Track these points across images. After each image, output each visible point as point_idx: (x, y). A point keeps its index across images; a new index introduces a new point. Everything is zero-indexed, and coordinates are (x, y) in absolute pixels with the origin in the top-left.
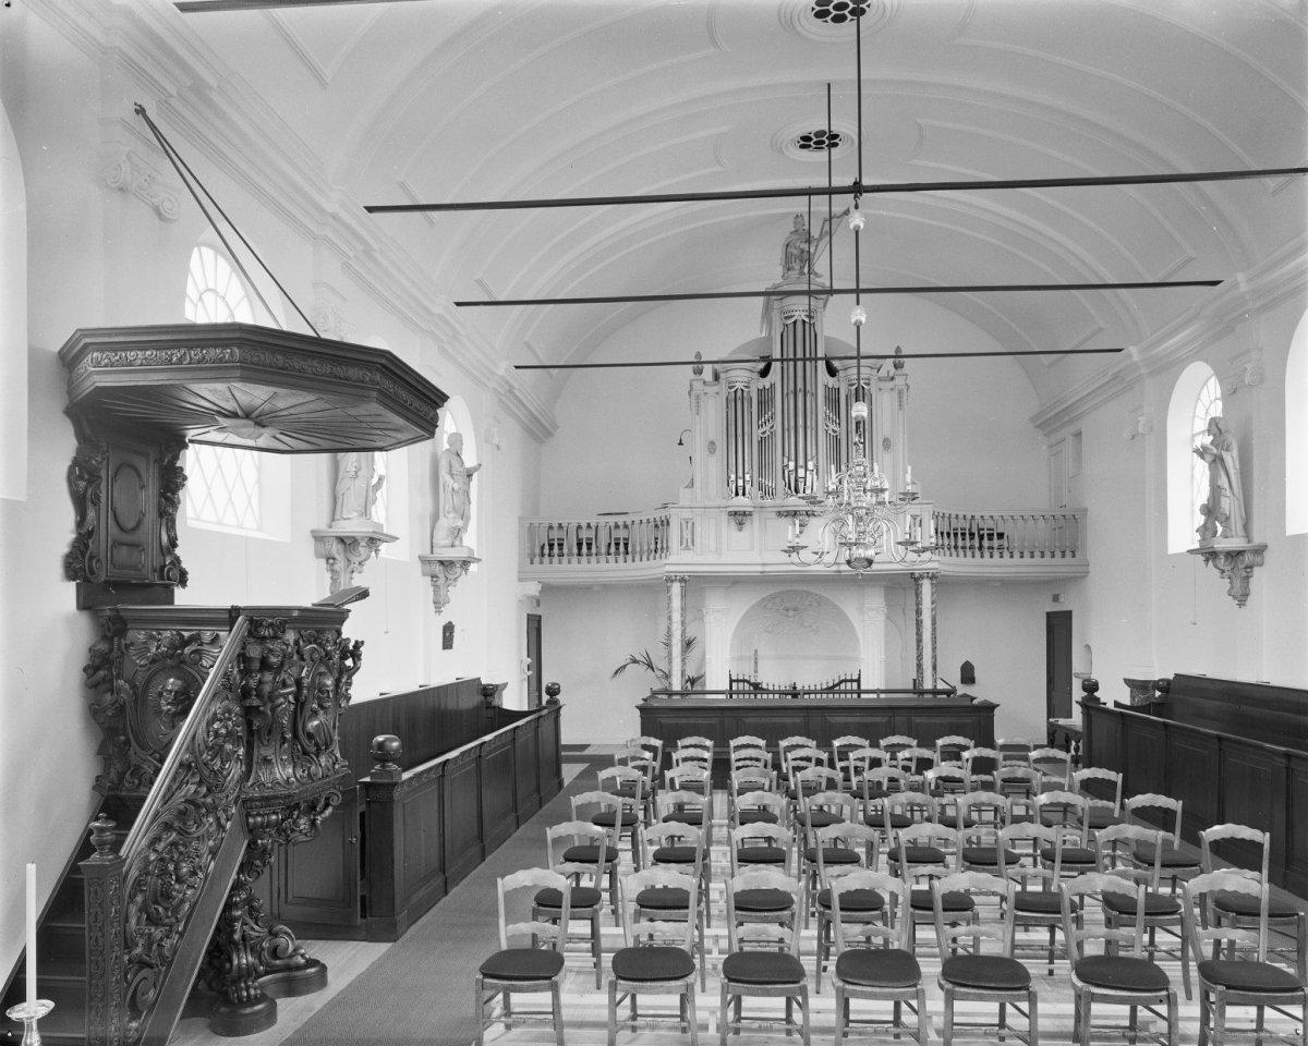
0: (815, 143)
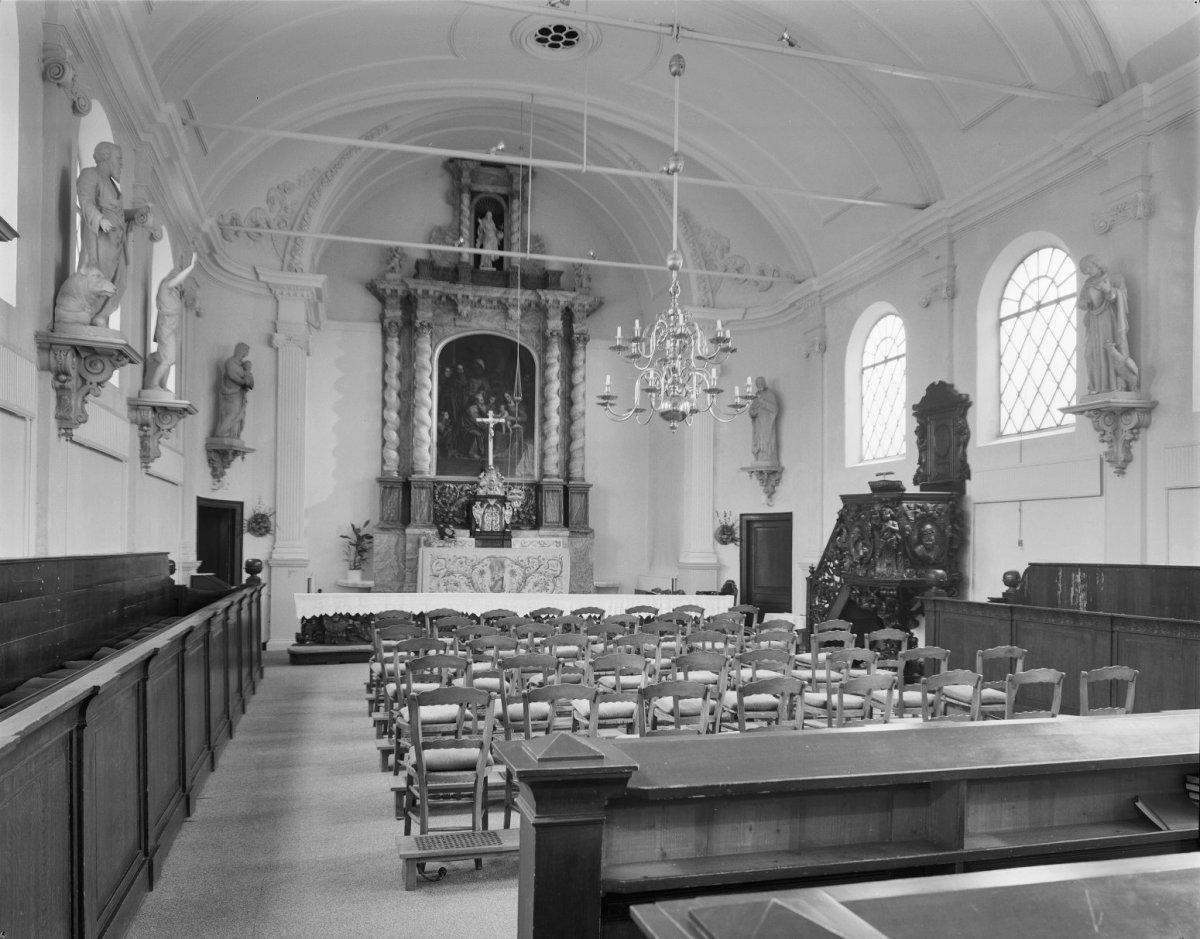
0: (553, 38)
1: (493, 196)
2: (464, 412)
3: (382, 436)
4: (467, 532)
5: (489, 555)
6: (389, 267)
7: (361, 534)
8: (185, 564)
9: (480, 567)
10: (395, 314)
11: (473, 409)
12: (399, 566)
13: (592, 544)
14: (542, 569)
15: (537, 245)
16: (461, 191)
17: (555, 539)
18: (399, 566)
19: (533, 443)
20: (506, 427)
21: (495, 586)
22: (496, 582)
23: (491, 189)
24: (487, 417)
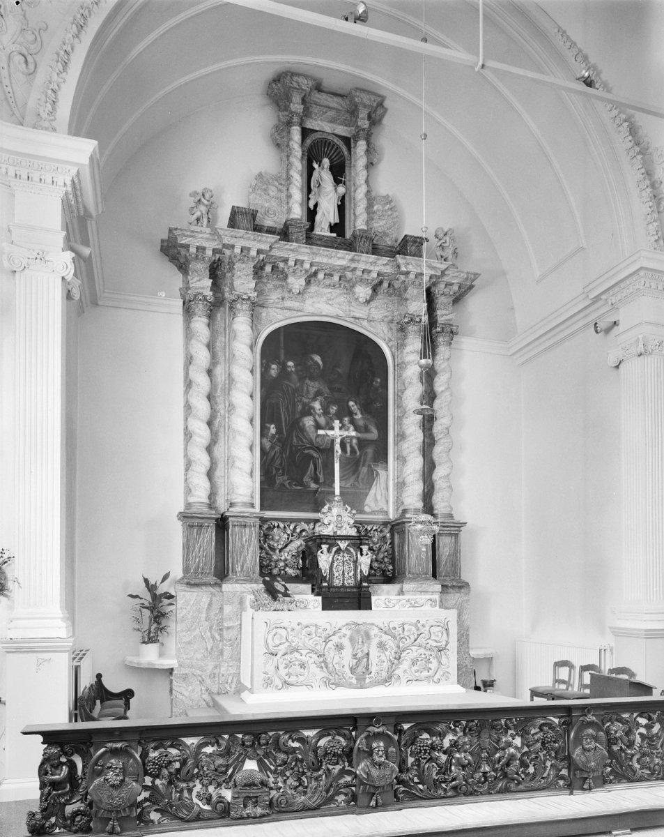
1: (331, 138)
2: (296, 426)
3: (186, 455)
4: (308, 587)
5: (348, 621)
6: (195, 217)
7: (159, 592)
8: (534, 697)
9: (335, 639)
10: (203, 284)
11: (308, 422)
12: (213, 638)
13: (468, 601)
14: (421, 640)
15: (387, 207)
16: (289, 124)
17: (428, 597)
18: (213, 638)
19: (386, 469)
20: (352, 447)
21: (357, 665)
22: (360, 660)
23: (327, 127)
24: (332, 428)
